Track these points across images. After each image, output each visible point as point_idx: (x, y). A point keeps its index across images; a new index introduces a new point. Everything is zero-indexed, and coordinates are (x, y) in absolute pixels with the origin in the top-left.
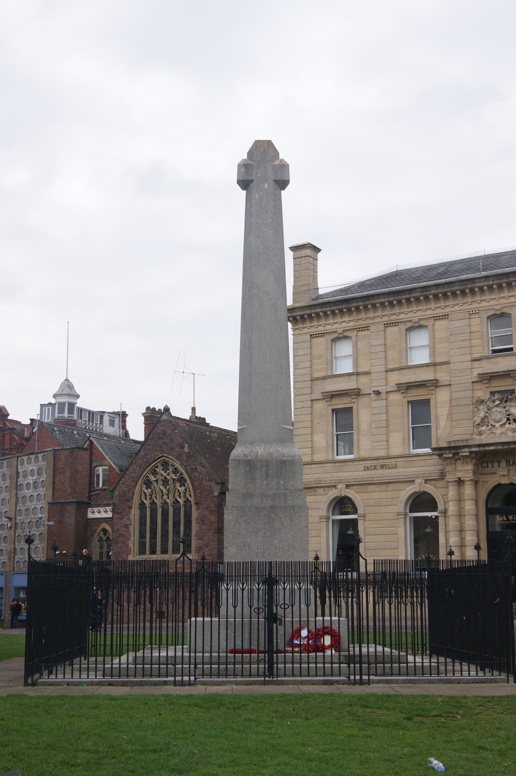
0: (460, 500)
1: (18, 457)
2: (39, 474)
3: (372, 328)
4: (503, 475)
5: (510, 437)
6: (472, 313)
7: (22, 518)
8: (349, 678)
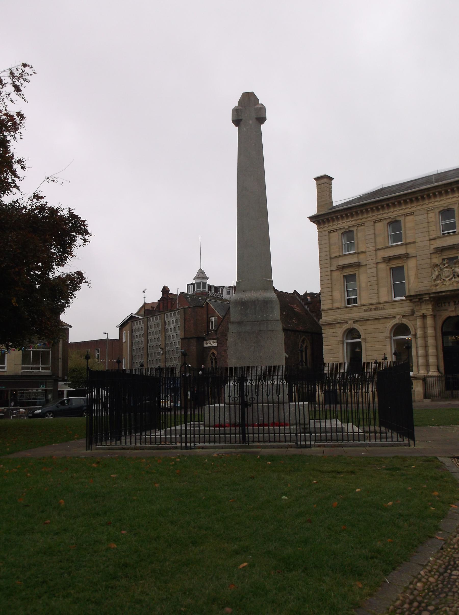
0: (424, 327)
1: (165, 313)
2: (177, 322)
3: (366, 224)
4: (451, 311)
5: (455, 287)
6: (428, 211)
7: (168, 348)
8: (297, 443)
